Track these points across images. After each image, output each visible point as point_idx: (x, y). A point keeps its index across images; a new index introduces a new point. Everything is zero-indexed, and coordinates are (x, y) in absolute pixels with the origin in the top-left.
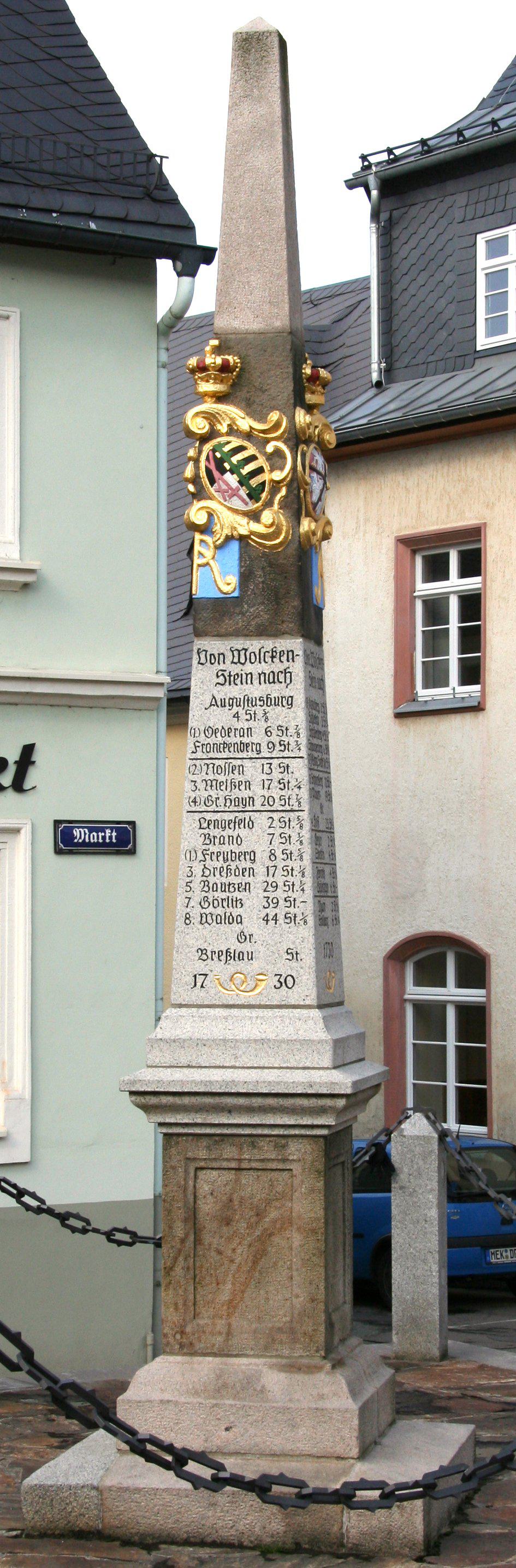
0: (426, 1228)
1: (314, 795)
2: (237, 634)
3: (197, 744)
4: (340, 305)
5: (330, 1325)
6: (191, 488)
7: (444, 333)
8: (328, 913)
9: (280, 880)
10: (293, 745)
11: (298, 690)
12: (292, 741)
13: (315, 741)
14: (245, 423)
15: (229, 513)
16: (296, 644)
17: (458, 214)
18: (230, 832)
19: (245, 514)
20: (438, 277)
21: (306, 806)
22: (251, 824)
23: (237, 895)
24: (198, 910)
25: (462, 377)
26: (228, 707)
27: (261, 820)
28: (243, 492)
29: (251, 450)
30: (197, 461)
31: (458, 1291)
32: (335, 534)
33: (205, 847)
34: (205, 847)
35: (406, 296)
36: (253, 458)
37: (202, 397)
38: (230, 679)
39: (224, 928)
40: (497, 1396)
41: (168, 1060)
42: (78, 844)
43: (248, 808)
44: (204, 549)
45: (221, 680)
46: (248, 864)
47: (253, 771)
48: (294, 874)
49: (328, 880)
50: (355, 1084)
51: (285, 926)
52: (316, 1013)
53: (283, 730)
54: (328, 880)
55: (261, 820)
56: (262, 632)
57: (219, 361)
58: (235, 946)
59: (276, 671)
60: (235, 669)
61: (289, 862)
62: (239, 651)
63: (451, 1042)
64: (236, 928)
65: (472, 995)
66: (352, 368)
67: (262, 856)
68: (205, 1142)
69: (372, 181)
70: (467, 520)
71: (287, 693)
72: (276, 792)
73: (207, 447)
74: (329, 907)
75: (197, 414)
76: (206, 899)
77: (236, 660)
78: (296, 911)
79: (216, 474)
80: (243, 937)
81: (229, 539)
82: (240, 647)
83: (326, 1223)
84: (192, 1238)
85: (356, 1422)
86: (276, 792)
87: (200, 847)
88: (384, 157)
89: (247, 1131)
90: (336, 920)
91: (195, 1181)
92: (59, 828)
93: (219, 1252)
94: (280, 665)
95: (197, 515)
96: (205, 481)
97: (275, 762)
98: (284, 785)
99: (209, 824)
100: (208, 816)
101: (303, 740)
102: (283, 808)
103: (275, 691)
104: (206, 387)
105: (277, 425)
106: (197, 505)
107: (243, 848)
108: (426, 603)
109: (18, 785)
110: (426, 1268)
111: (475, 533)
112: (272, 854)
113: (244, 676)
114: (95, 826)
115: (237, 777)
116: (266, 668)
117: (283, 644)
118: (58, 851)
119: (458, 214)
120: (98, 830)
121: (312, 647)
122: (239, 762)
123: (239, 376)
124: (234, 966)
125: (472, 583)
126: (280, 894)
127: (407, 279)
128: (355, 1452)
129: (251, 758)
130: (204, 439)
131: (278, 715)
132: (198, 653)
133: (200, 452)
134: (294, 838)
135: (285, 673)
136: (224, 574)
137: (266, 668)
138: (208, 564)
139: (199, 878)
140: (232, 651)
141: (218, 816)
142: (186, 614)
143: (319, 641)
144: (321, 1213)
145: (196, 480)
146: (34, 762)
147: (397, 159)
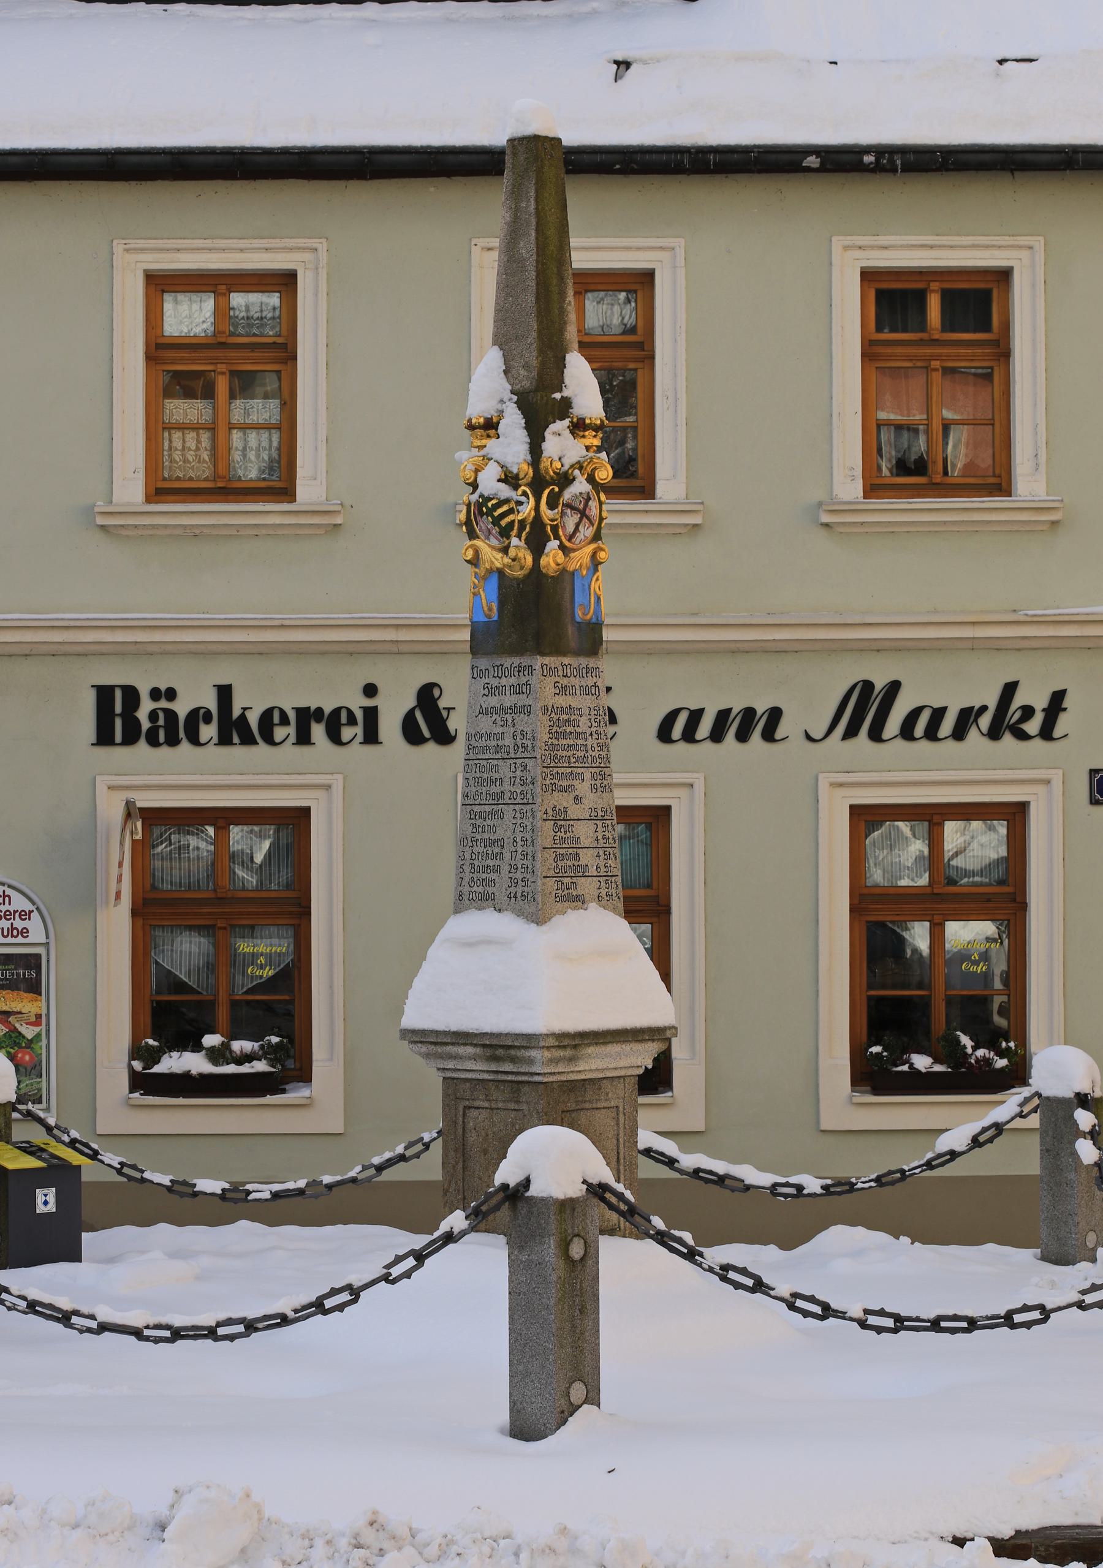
0: (1066, 1191)
3: (470, 747)
18: (488, 822)
24: (466, 889)
26: (490, 715)
27: (508, 811)
28: (495, 530)
33: (473, 835)
34: (473, 835)
38: (492, 691)
43: (500, 802)
46: (497, 850)
51: (521, 903)
55: (508, 811)
59: (521, 683)
60: (495, 682)
76: (472, 879)
77: (496, 675)
81: (490, 571)
82: (498, 663)
84: (460, 1165)
91: (464, 1118)
92: (1095, 777)
94: (523, 678)
97: (519, 761)
98: (524, 783)
99: (476, 815)
100: (476, 809)
102: (523, 802)
103: (521, 700)
107: (496, 837)
109: (1047, 733)
110: (1067, 1230)
113: (501, 688)
115: (495, 776)
116: (513, 681)
117: (525, 661)
122: (496, 762)
126: (519, 876)
129: (503, 759)
137: (513, 681)
139: (468, 862)
146: (1065, 709)
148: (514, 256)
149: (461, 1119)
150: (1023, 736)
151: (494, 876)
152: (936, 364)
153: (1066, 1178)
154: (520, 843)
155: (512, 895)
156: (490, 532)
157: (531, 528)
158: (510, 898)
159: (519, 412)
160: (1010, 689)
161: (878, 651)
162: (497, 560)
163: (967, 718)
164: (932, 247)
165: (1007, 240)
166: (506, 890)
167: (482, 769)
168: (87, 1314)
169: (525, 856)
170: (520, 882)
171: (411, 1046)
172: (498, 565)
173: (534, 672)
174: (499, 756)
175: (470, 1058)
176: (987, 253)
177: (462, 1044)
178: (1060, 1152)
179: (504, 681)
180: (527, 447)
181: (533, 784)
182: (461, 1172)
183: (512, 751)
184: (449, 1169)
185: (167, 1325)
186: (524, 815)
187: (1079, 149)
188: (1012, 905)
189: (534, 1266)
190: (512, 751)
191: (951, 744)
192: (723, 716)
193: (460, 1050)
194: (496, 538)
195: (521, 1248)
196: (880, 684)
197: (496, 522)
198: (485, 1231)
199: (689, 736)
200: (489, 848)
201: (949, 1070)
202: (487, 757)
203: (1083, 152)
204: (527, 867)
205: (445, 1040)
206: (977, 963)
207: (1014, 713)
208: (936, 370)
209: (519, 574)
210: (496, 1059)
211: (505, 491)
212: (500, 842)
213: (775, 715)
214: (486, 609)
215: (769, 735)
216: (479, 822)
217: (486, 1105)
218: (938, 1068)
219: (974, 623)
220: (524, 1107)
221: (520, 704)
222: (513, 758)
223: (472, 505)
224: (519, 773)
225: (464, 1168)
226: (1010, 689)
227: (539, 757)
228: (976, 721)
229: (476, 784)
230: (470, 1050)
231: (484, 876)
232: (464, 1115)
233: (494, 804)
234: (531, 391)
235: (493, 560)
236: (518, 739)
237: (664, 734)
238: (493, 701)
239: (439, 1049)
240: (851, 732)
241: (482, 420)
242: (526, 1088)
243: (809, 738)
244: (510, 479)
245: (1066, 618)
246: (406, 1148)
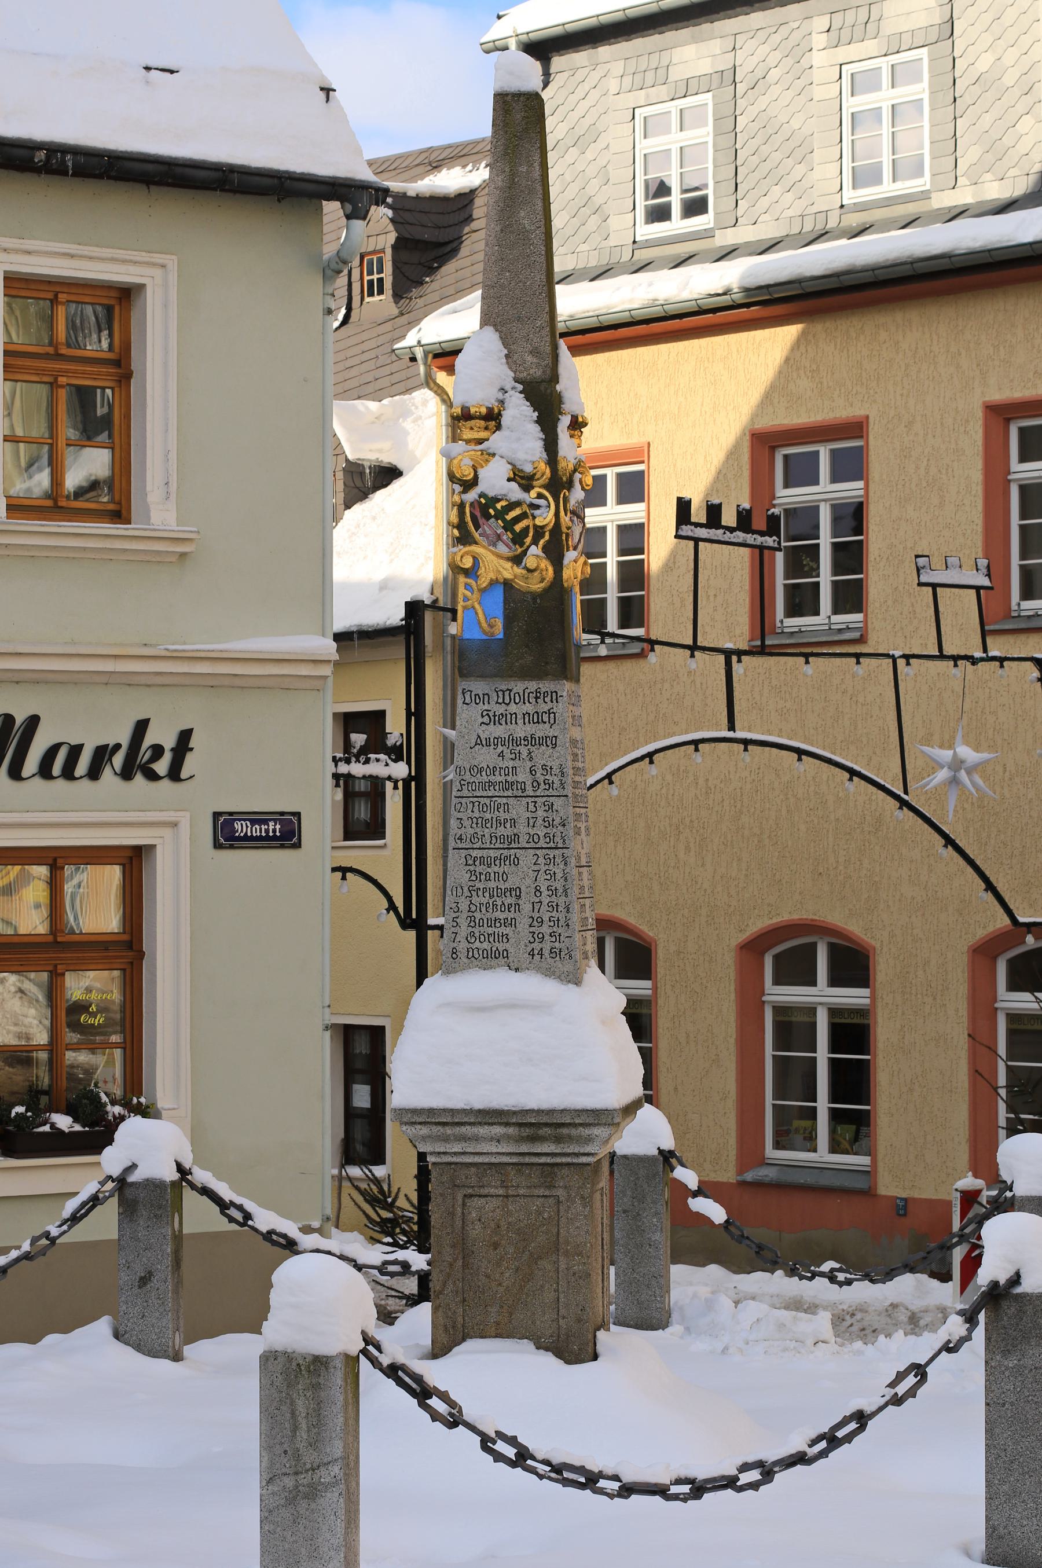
3: (463, 782)
12: (556, 780)
23: (503, 930)
27: (527, 858)
28: (507, 536)
33: (470, 883)
34: (470, 883)
38: (495, 719)
42: (239, 839)
43: (513, 845)
45: (486, 719)
46: (508, 901)
47: (519, 810)
48: (559, 910)
55: (527, 858)
56: (526, 674)
60: (501, 709)
62: (503, 692)
65: (852, 996)
70: (634, 440)
77: (500, 700)
78: (562, 945)
79: (481, 521)
81: (493, 583)
82: (504, 688)
84: (460, 1263)
93: (488, 1276)
97: (540, 800)
98: (549, 824)
99: (474, 861)
100: (474, 853)
102: (549, 846)
103: (541, 730)
107: (507, 885)
110: (650, 1293)
112: (537, 890)
113: (509, 716)
114: (258, 818)
115: (503, 816)
116: (529, 708)
117: (546, 686)
122: (504, 800)
126: (545, 929)
129: (516, 797)
132: (463, 694)
134: (559, 875)
135: (549, 714)
137: (529, 708)
139: (465, 915)
140: (497, 692)
141: (485, 853)
146: (192, 749)
148: (510, 225)
149: (459, 1210)
150: (152, 776)
151: (507, 930)
152: (62, 380)
153: (649, 1239)
154: (545, 893)
155: (536, 952)
156: (499, 537)
157: (550, 535)
158: (533, 955)
159: (528, 404)
160: (141, 727)
161: (17, 683)
162: (505, 569)
163: (102, 755)
164: (72, 256)
165: (144, 257)
166: (526, 946)
167: (483, 808)
168: (610, 1474)
169: (554, 907)
170: (547, 937)
171: (404, 1128)
173: (560, 699)
174: (510, 793)
175: (492, 1139)
176: (122, 268)
177: (485, 1124)
178: (640, 1213)
179: (513, 708)
180: (541, 444)
181: (564, 825)
182: (461, 1270)
183: (529, 788)
184: (442, 1268)
185: (686, 1478)
186: (550, 861)
187: (236, 169)
188: (130, 954)
189: (1026, 1372)
190: (529, 788)
191: (86, 783)
193: (483, 1131)
194: (507, 546)
195: (1006, 1353)
196: (19, 719)
197: (508, 526)
198: (496, 1337)
200: (498, 899)
201: (87, 1129)
202: (490, 795)
203: (238, 172)
204: (558, 920)
205: (466, 1120)
206: (93, 1015)
207: (144, 754)
208: (62, 387)
209: (536, 586)
210: (533, 1139)
211: (515, 492)
212: (516, 892)
214: (484, 625)
216: (479, 869)
217: (501, 1192)
218: (78, 1128)
219: (116, 657)
220: (560, 1193)
221: (540, 734)
222: (532, 797)
223: (467, 506)
224: (540, 813)
225: (465, 1266)
226: (141, 727)
227: (570, 795)
228: (110, 759)
229: (474, 825)
230: (498, 1130)
231: (490, 930)
232: (464, 1204)
233: (504, 849)
234: (543, 381)
235: (501, 570)
236: (538, 775)
238: (499, 731)
239: (449, 1131)
241: (484, 410)
242: (565, 1171)
244: (524, 480)
245: (203, 655)
246: (32, 1244)
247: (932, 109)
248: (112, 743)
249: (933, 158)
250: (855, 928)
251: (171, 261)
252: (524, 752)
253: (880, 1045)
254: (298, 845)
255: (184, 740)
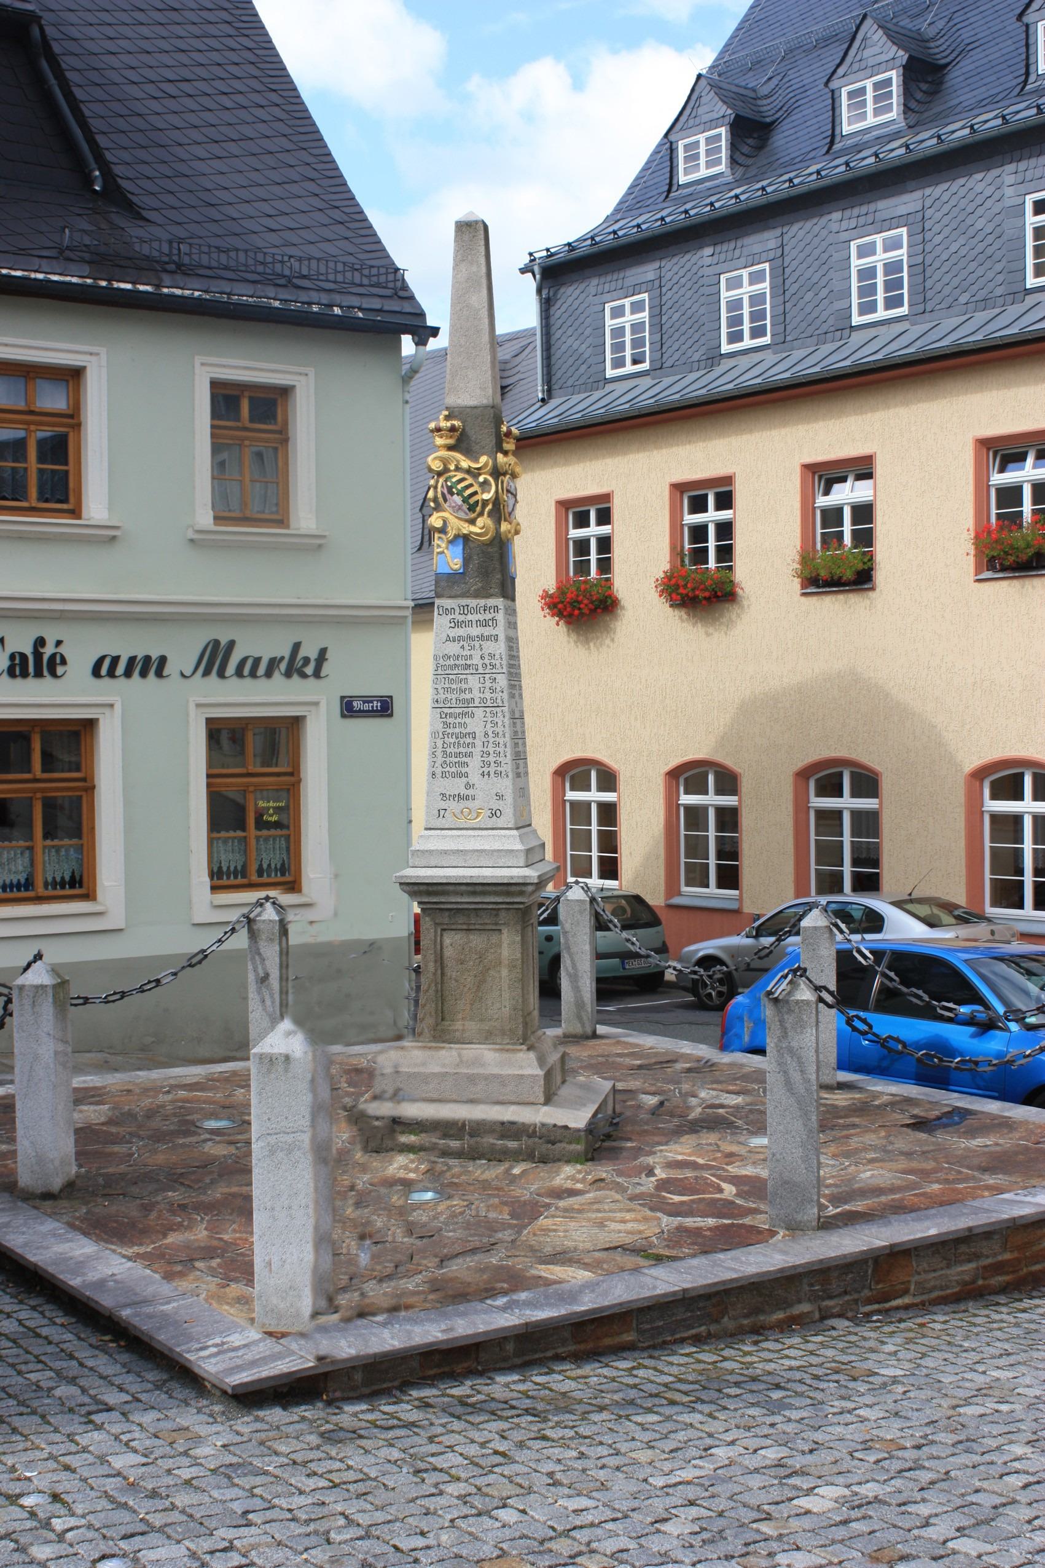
1: (512, 696)
2: (464, 595)
4: (516, 346)
5: (526, 1024)
6: (432, 504)
7: (584, 367)
8: (521, 770)
9: (491, 751)
10: (498, 665)
11: (500, 631)
12: (498, 663)
13: (512, 662)
14: (465, 464)
15: (456, 520)
16: (499, 602)
17: (593, 290)
19: (467, 521)
20: (580, 331)
21: (506, 704)
22: (473, 715)
24: (440, 769)
25: (597, 395)
27: (479, 713)
28: (465, 507)
29: (470, 481)
30: (436, 488)
31: (603, 986)
32: (523, 527)
35: (560, 342)
36: (471, 485)
37: (438, 448)
38: (458, 624)
39: (457, 780)
40: (628, 1061)
41: (424, 863)
42: (356, 711)
44: (439, 543)
45: (452, 625)
46: (468, 740)
47: (473, 682)
49: (521, 748)
50: (539, 877)
52: (515, 832)
53: (492, 656)
54: (521, 748)
55: (479, 713)
56: (477, 595)
57: (449, 424)
58: (464, 792)
60: (461, 618)
61: (497, 739)
63: (594, 828)
64: (464, 780)
65: (609, 797)
66: (525, 387)
67: (480, 734)
68: (447, 914)
69: (536, 269)
71: (494, 632)
72: (488, 695)
73: (441, 480)
74: (522, 766)
75: (435, 458)
79: (448, 496)
80: (468, 786)
81: (456, 537)
83: (523, 962)
84: (439, 972)
85: (542, 1082)
86: (488, 695)
87: (441, 730)
88: (544, 253)
89: (473, 906)
90: (527, 773)
93: (457, 981)
95: (435, 521)
96: (441, 500)
97: (487, 676)
98: (493, 690)
100: (446, 710)
101: (504, 662)
103: (487, 631)
104: (439, 441)
105: (486, 465)
106: (436, 515)
107: (468, 730)
108: (575, 542)
109: (317, 674)
111: (607, 497)
112: (486, 734)
114: (367, 699)
115: (464, 686)
117: (491, 602)
118: (343, 716)
119: (593, 290)
120: (368, 702)
121: (509, 603)
123: (461, 434)
124: (463, 804)
125: (605, 530)
126: (492, 759)
127: (560, 331)
128: (542, 1100)
130: (439, 474)
131: (489, 647)
133: (437, 482)
134: (500, 724)
136: (453, 558)
138: (443, 552)
141: (452, 710)
142: (419, 549)
143: (513, 599)
144: (519, 955)
145: (435, 500)
147: (552, 255)
150: (304, 676)
160: (297, 647)
163: (273, 663)
167: (451, 681)
172: (465, 532)
179: (470, 617)
183: (480, 666)
190: (480, 666)
191: (264, 680)
192: (132, 660)
196: (224, 642)
199: (111, 674)
207: (299, 663)
213: (163, 660)
215: (159, 674)
217: (465, 927)
226: (297, 647)
237: (96, 672)
240: (207, 673)
243: (183, 675)
247: (772, 297)
248: (279, 656)
249: (772, 325)
250: (729, 762)
251: (311, 371)
252: (477, 645)
253: (744, 828)
254: (391, 715)
255: (322, 654)
